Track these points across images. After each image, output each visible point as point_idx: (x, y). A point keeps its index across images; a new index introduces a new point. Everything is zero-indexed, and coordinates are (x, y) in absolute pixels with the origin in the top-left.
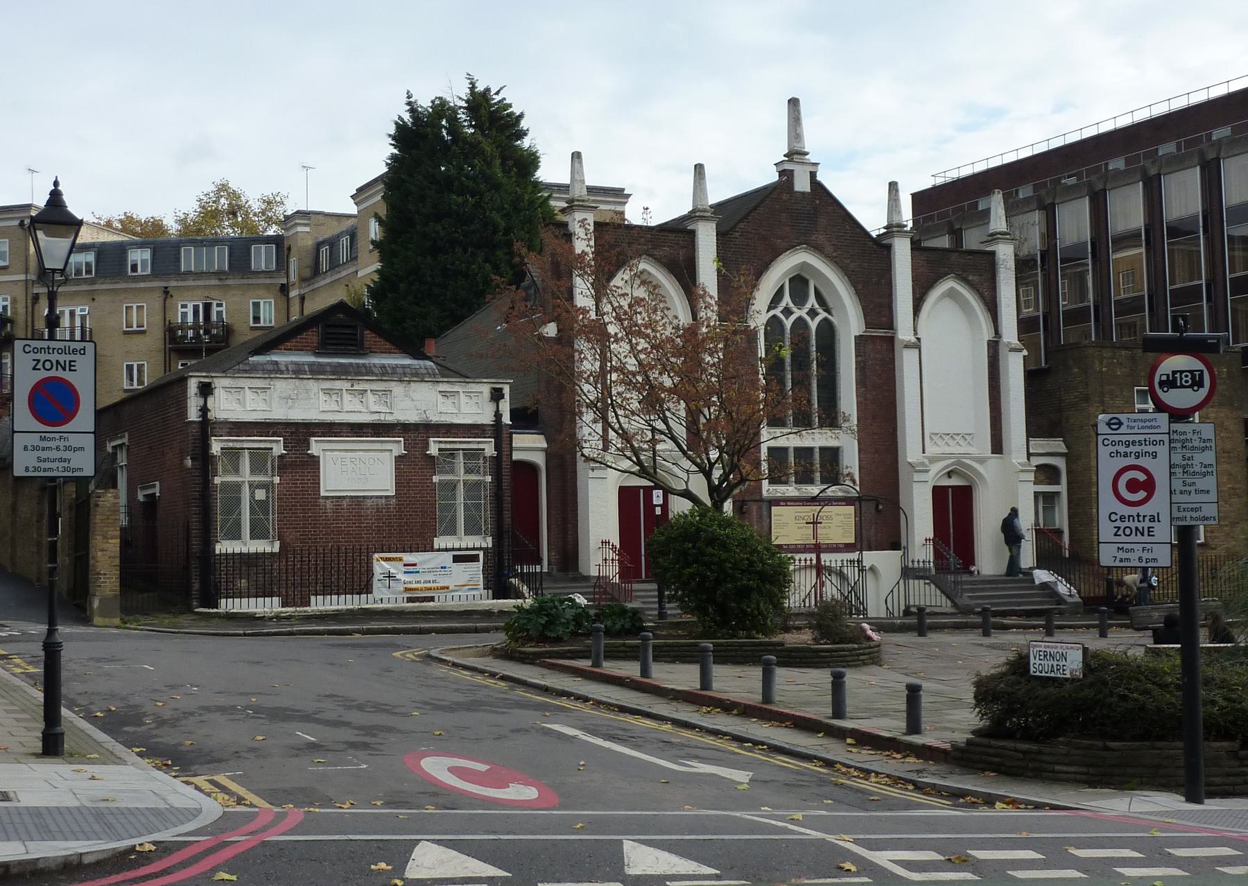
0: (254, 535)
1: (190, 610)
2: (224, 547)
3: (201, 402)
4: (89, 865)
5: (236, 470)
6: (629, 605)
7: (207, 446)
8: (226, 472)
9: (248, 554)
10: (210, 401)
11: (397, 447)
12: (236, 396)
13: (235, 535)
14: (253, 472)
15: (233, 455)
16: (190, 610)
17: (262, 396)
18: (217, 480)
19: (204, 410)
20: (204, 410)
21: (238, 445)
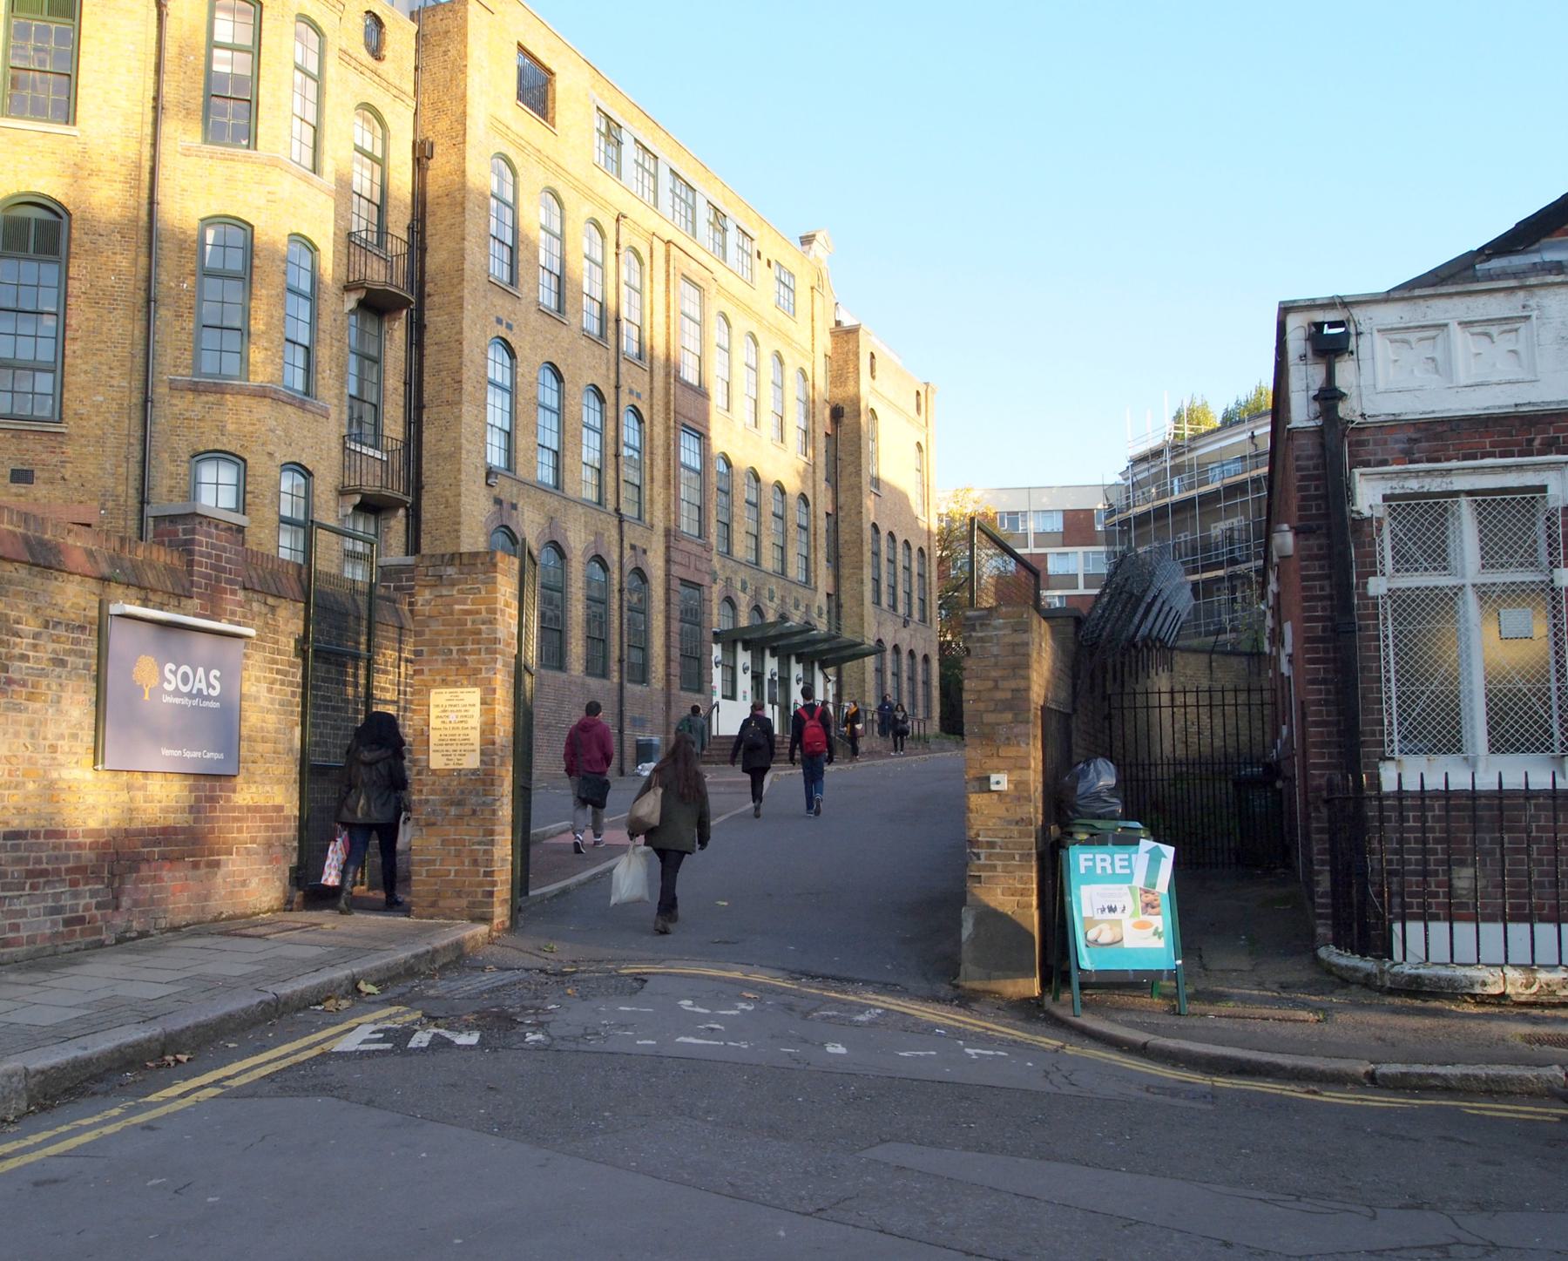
0: (1501, 742)
1: (1306, 946)
2: (1406, 772)
3: (1317, 374)
4: (459, 1046)
5: (1438, 557)
6: (387, 656)
7: (1344, 493)
8: (1404, 562)
9: (1473, 795)
10: (1345, 375)
11: (753, 559)
12: (1425, 350)
13: (1449, 741)
14: (1489, 560)
15: (1424, 517)
16: (1306, 946)
17: (1504, 343)
18: (1377, 586)
19: (1329, 396)
20: (1329, 396)
21: (1435, 485)
